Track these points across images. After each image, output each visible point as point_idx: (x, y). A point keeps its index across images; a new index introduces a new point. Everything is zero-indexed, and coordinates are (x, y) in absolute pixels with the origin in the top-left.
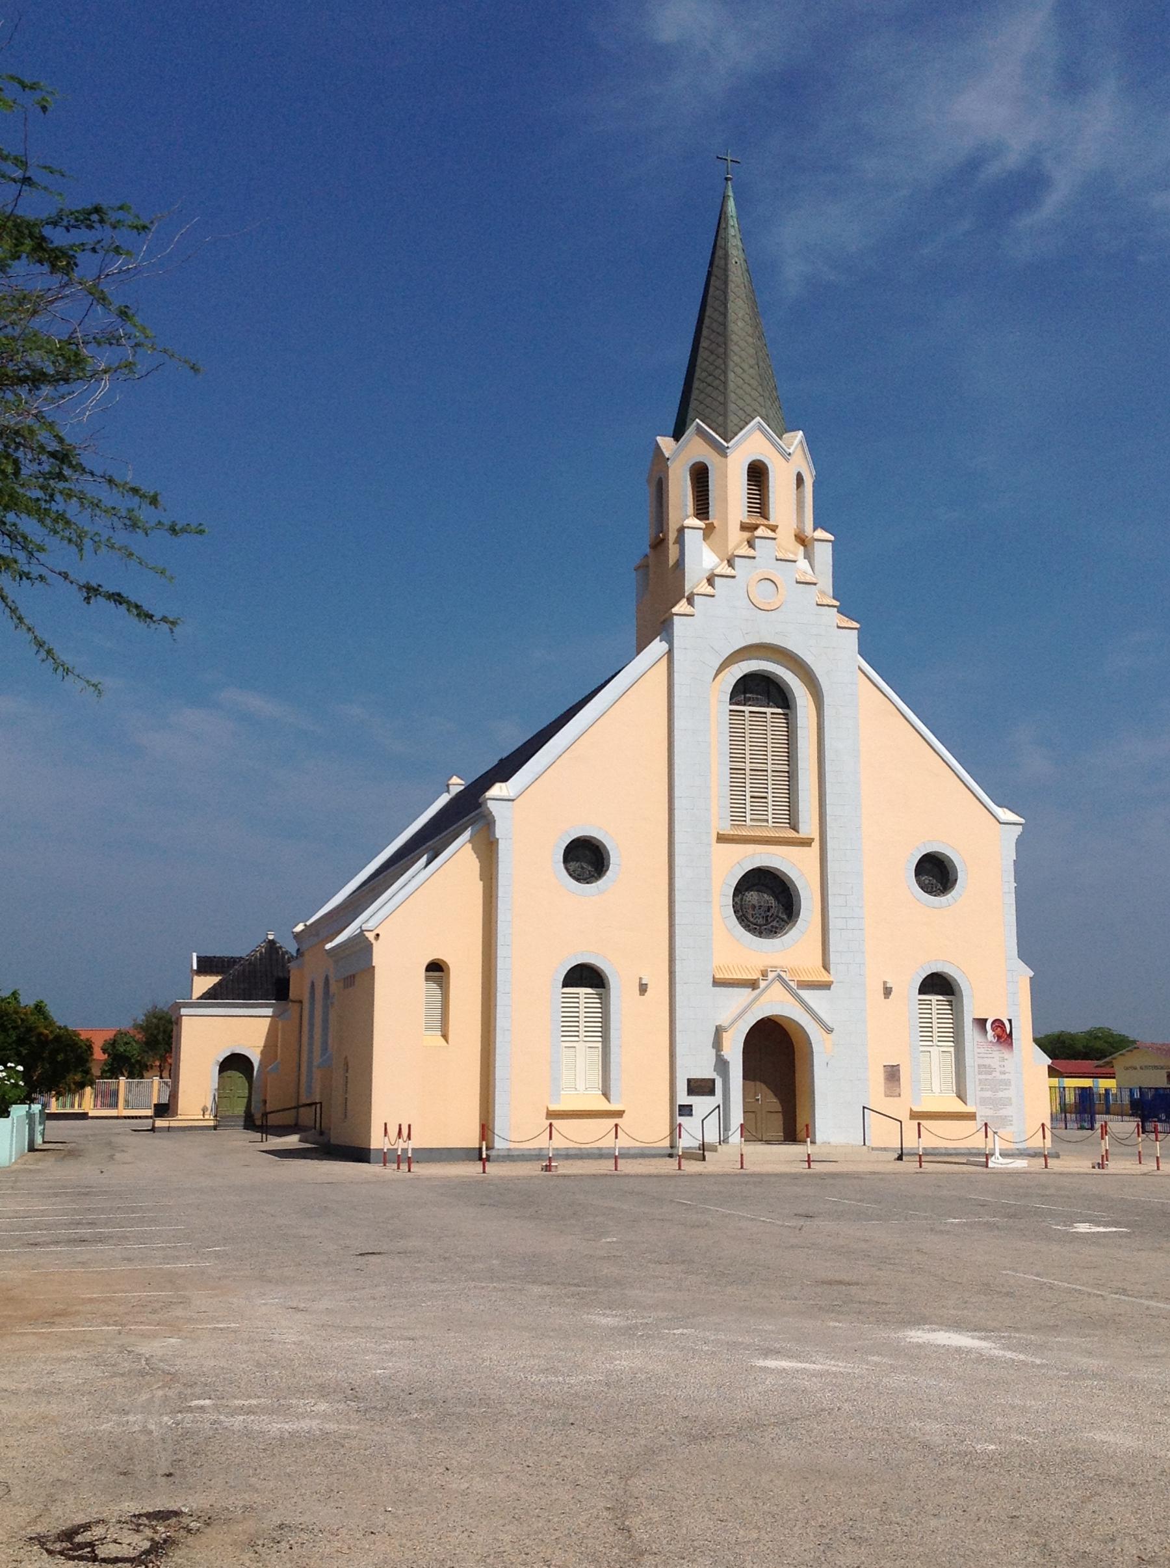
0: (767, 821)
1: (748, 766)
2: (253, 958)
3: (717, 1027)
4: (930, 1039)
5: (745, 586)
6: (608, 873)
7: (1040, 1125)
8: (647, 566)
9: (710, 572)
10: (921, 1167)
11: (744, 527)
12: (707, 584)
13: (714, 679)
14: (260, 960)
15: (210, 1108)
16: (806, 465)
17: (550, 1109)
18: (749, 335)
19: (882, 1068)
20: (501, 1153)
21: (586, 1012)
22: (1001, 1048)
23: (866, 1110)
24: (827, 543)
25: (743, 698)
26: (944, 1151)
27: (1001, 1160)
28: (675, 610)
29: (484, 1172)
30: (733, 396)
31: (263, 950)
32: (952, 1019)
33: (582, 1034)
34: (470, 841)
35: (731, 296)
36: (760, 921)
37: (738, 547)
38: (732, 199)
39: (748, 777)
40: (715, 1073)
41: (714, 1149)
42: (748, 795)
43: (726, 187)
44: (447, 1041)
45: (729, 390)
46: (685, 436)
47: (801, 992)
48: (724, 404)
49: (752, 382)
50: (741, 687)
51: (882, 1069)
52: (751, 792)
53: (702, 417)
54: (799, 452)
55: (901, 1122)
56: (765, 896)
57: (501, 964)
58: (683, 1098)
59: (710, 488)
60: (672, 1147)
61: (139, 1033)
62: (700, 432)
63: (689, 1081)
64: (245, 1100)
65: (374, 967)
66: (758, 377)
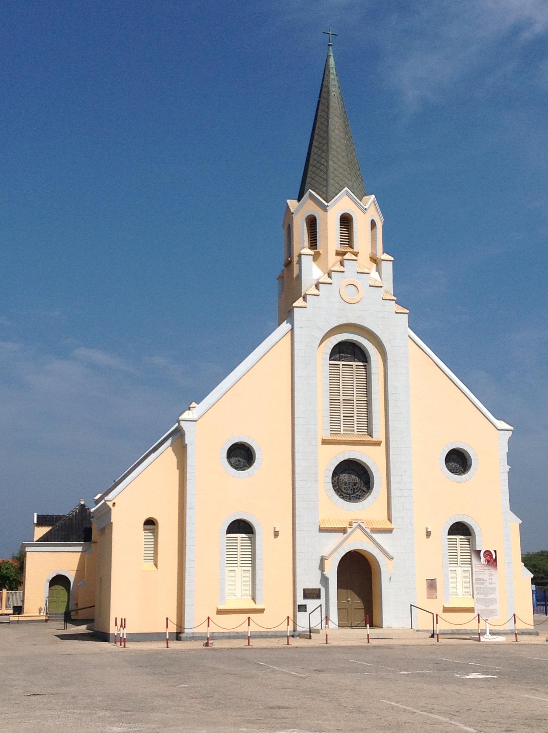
0: (354, 431)
1: (341, 398)
2: (71, 516)
3: (321, 557)
4: (456, 562)
5: (338, 289)
6: (255, 464)
9: (317, 281)
11: (338, 254)
12: (315, 288)
16: (377, 215)
17: (219, 608)
18: (342, 138)
21: (241, 549)
22: (490, 568)
23: (412, 607)
24: (310, 256)
26: (464, 632)
27: (490, 637)
28: (295, 304)
29: (167, 647)
30: (331, 175)
31: (78, 511)
33: (239, 562)
34: (171, 446)
35: (331, 115)
36: (350, 492)
37: (334, 265)
38: (332, 57)
39: (342, 404)
40: (321, 585)
41: (317, 632)
42: (342, 415)
43: (329, 50)
44: (157, 567)
47: (373, 535)
48: (326, 180)
50: (337, 350)
51: (425, 582)
52: (343, 413)
54: (373, 208)
55: (309, 614)
56: (353, 476)
57: (188, 520)
58: (301, 601)
59: (318, 230)
60: (294, 631)
61: (16, 562)
62: (312, 197)
63: (304, 590)
65: (112, 523)
66: (347, 164)
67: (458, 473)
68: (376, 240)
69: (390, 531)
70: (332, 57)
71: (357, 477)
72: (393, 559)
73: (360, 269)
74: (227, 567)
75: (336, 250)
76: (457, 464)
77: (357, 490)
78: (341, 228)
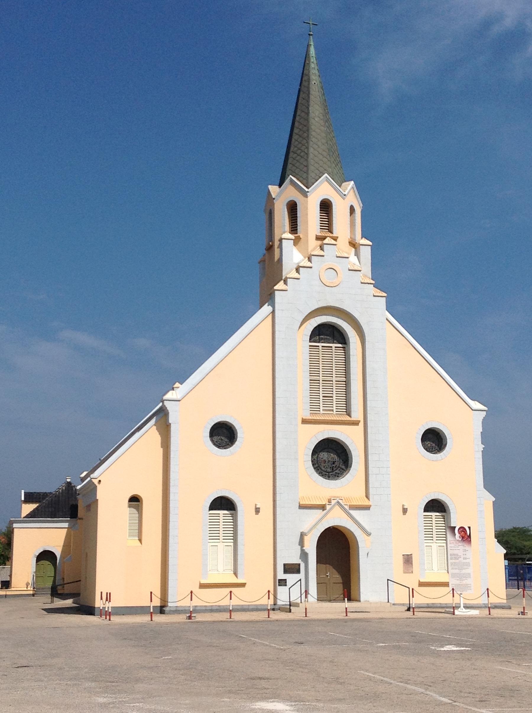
0: (333, 410)
1: (321, 378)
2: (57, 493)
3: (301, 533)
4: (432, 538)
5: (318, 273)
6: (237, 443)
7: (267, 591)
8: (264, 261)
9: (297, 265)
10: (414, 614)
11: (318, 238)
13: (299, 328)
14: (62, 493)
15: (31, 584)
17: (421, 581)
19: (402, 556)
20: (172, 609)
23: (389, 581)
25: (318, 338)
26: (439, 605)
27: (464, 610)
28: (276, 288)
31: (64, 488)
32: (445, 526)
33: (221, 538)
34: (155, 425)
35: (311, 103)
36: (329, 470)
37: (314, 249)
38: (312, 46)
39: (321, 385)
41: (297, 605)
42: (321, 395)
43: (309, 40)
45: (309, 158)
46: (285, 183)
47: (352, 512)
49: (324, 153)
50: (317, 332)
53: (294, 174)
58: (281, 575)
59: (298, 215)
60: (274, 605)
62: (292, 182)
63: (285, 565)
64: (53, 578)
67: (434, 452)
68: (355, 225)
69: (368, 508)
70: (312, 46)
71: (335, 456)
72: (370, 535)
73: (339, 253)
74: (209, 542)
75: (316, 235)
76: (433, 442)
77: (336, 468)
78: (320, 213)
